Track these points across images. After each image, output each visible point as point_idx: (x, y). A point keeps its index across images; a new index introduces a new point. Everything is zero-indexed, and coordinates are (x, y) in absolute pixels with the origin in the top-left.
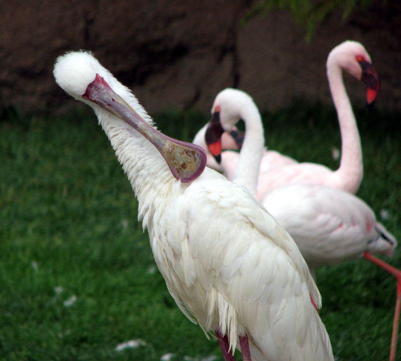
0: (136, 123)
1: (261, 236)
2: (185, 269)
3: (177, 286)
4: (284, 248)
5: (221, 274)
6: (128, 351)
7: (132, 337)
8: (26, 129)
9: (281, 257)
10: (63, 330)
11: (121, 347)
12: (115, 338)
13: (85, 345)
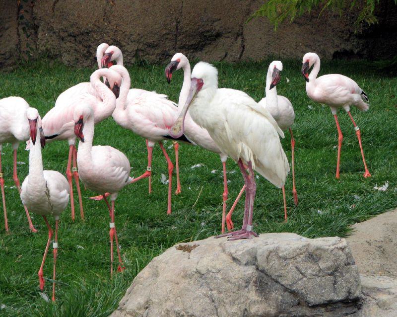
1: (256, 114)
5: (243, 135)
6: (196, 168)
7: (197, 163)
8: (150, 70)
9: (267, 121)
11: (193, 167)
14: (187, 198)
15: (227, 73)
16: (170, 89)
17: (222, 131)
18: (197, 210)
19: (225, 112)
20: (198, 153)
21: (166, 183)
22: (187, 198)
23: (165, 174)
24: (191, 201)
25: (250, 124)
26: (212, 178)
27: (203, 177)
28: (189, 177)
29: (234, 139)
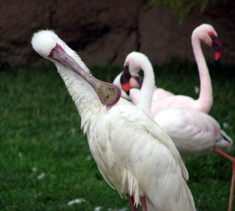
1: (153, 138)
2: (109, 157)
3: (104, 167)
4: (166, 145)
5: (129, 160)
6: (75, 205)
7: (77, 197)
8: (15, 75)
9: (165, 150)
10: (37, 193)
11: (71, 203)
12: (67, 197)
13: (50, 202)
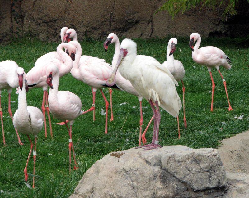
0: (155, 167)
1: (161, 71)
5: (153, 84)
6: (123, 105)
7: (124, 102)
8: (94, 44)
11: (121, 104)
14: (117, 124)
15: (142, 45)
16: (107, 55)
17: (139, 82)
18: (123, 131)
19: (141, 70)
20: (124, 96)
21: (104, 114)
22: (117, 124)
23: (103, 108)
24: (120, 125)
25: (157, 78)
26: (133, 111)
27: (127, 111)
28: (119, 111)
29: (147, 87)
